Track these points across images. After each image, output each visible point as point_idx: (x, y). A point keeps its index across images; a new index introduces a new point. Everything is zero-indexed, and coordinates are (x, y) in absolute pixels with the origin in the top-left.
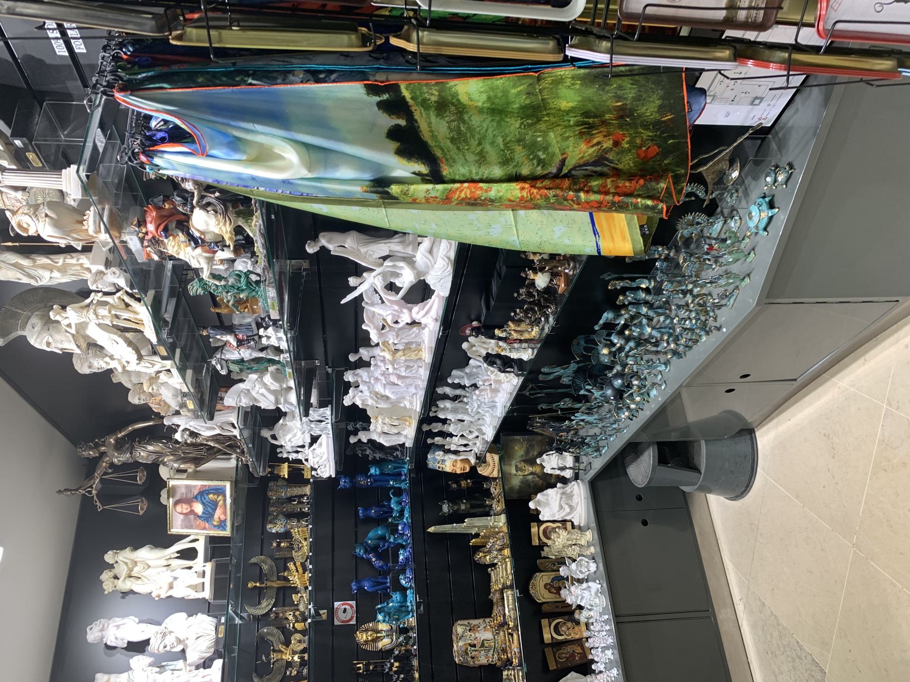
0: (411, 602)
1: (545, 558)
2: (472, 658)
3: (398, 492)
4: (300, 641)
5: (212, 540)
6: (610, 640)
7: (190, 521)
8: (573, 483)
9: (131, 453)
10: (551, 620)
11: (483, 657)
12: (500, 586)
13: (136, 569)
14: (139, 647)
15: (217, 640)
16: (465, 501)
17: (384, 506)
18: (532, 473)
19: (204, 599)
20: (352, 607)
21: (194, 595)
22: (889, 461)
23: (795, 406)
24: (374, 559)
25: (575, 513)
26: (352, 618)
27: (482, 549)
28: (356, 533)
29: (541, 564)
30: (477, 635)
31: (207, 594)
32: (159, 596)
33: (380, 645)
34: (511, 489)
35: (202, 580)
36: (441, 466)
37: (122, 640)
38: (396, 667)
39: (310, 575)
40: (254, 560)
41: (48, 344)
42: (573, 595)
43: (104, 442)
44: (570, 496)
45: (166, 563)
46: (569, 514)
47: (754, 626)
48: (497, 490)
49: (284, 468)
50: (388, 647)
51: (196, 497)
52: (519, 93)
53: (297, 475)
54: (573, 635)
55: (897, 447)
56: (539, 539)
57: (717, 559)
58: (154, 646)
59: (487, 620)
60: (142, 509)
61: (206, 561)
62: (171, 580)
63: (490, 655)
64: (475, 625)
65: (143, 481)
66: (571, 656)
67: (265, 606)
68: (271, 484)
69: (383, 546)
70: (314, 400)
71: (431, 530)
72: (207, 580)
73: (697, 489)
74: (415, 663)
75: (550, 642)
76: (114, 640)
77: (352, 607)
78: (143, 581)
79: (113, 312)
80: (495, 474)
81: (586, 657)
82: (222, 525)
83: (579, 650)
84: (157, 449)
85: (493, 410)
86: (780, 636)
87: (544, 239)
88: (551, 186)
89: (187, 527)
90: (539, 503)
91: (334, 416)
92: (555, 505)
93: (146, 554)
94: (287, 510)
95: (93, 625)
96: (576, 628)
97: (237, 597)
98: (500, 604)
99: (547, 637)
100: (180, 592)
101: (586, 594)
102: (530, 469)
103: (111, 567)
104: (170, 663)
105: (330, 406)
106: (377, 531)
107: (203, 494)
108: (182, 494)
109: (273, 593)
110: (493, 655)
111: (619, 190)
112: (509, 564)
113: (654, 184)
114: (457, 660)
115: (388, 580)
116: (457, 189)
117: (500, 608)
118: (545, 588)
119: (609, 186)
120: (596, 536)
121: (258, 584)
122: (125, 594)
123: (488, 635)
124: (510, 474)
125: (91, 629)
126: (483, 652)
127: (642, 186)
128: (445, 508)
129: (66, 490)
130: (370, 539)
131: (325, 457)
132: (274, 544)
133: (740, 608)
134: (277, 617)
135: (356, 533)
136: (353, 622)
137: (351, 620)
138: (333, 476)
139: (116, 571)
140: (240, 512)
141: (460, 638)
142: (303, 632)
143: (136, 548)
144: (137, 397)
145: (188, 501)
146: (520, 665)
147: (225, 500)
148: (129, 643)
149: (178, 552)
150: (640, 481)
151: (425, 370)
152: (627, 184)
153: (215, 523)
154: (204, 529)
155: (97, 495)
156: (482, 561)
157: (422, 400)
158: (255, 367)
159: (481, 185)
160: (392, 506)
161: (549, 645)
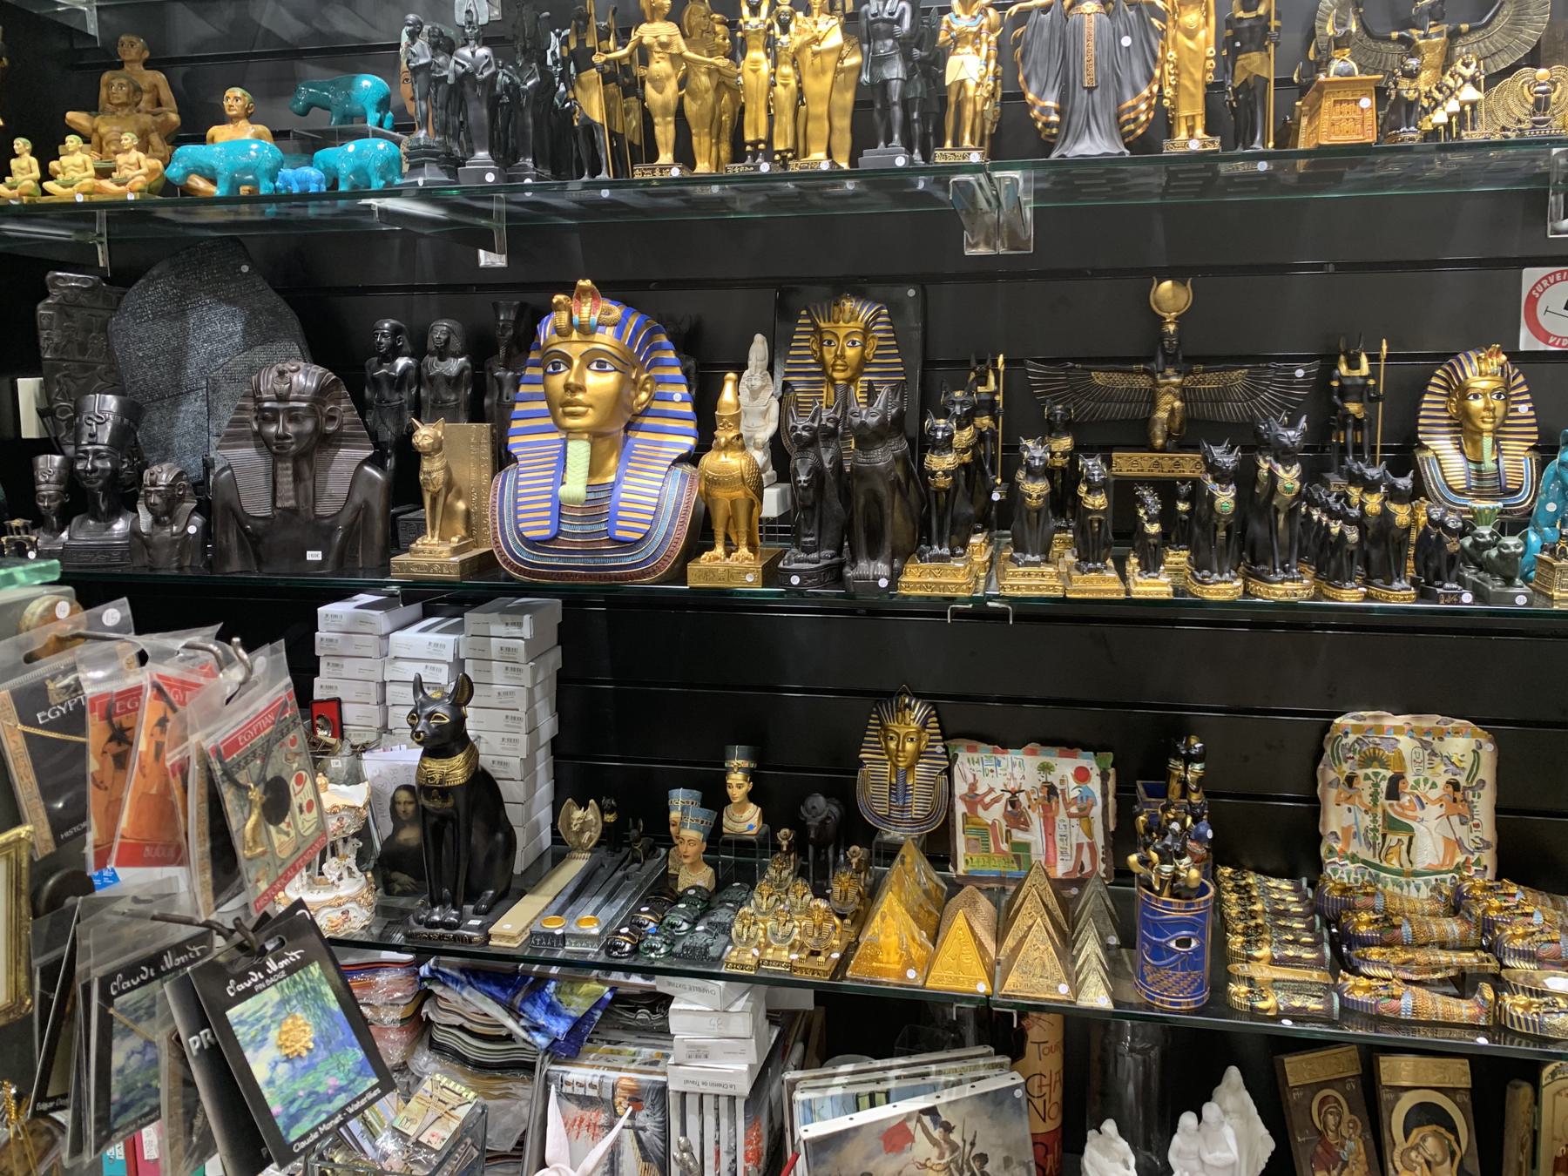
2: (1350, 780)
10: (1467, 1099)
11: (1348, 820)
30: (1434, 811)
38: (1273, 477)
52: (1266, 461)
59: (1488, 858)
63: (1355, 847)
64: (1471, 807)
66: (1328, 1148)
75: (1385, 1079)
123: (1429, 849)
136: (1527, 341)
137: (1539, 332)
141: (1425, 745)
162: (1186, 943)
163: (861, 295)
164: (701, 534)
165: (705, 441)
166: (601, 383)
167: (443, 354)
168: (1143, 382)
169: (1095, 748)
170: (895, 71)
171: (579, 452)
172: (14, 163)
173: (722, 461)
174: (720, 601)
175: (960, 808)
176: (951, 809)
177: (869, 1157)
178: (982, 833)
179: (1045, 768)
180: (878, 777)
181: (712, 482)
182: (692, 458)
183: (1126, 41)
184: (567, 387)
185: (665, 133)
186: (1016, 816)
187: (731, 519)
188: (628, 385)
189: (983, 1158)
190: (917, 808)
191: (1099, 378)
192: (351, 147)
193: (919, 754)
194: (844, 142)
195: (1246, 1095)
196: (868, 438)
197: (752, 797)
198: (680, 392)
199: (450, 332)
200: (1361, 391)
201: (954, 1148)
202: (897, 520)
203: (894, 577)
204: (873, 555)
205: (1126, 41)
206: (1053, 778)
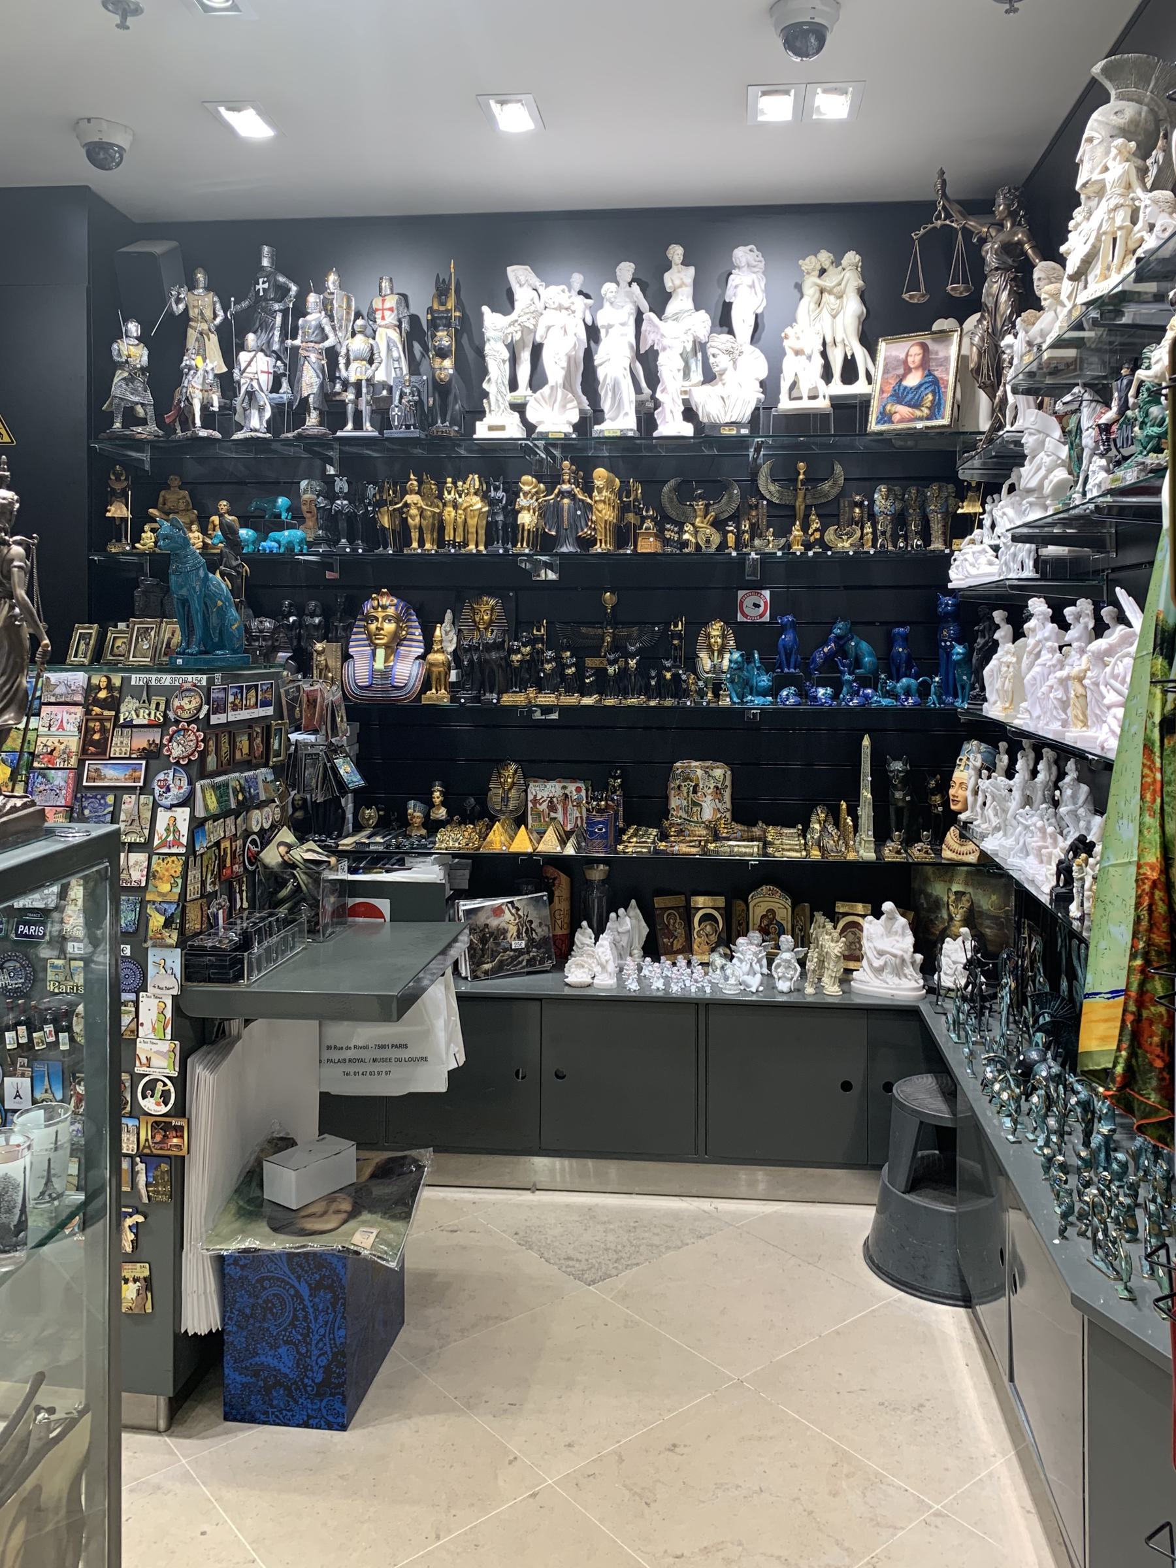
0: (752, 701)
1: (812, 917)
2: (679, 787)
3: (924, 691)
4: (708, 541)
5: (864, 403)
6: (675, 989)
7: (895, 369)
8: (921, 982)
9: (997, 269)
10: (723, 912)
11: (678, 802)
12: (770, 838)
13: (832, 298)
14: (724, 321)
15: (716, 426)
16: (908, 798)
17: (909, 667)
18: (951, 919)
19: (778, 401)
20: (761, 616)
21: (785, 386)
22: (847, 1476)
23: (988, 1382)
24: (826, 650)
25: (872, 975)
26: (746, 616)
27: (831, 819)
28: (872, 623)
29: (803, 909)
30: (709, 798)
31: (786, 404)
32: (786, 337)
33: (703, 655)
34: (926, 880)
35: (805, 396)
36: (963, 764)
37: (735, 295)
39: (798, 553)
40: (838, 469)
41: (1090, 140)
42: (748, 947)
43: (1020, 224)
44: (898, 971)
45: (838, 340)
46: (871, 965)
47: (676, 1215)
48: (917, 853)
49: (974, 506)
50: (699, 668)
51: (930, 374)
53: (963, 527)
54: (698, 940)
55: (864, 1493)
56: (845, 914)
57: (781, 1193)
58: (722, 340)
59: (728, 815)
60: (911, 297)
61: (832, 398)
62: (807, 351)
63: (681, 813)
64: (723, 796)
65: (952, 293)
66: (669, 930)
67: (769, 489)
68: (951, 488)
69: (843, 664)
70: (1052, 550)
71: (866, 742)
72: (805, 404)
73: (884, 1185)
74: (668, 702)
76: (734, 284)
77: (761, 616)
78: (814, 311)
79: (1119, 233)
80: (947, 854)
81: (665, 954)
82: (885, 417)
83: (677, 945)
84: (1002, 307)
85: (1021, 851)
86: (652, 1245)
87: (1109, 908)
88: (1156, 914)
89: (886, 365)
90: (892, 919)
91: (1016, 583)
92: (886, 944)
93: (853, 307)
94: (911, 515)
95: (757, 253)
96: (707, 947)
97: (782, 447)
98: (745, 835)
99: (700, 901)
100: (791, 367)
101: (746, 967)
102: (958, 917)
103: (837, 262)
104: (700, 364)
105: (1038, 576)
106: (870, 655)
107: (934, 383)
108: (937, 353)
109: (787, 501)
110: (680, 818)
111: (1145, 1024)
112: (798, 855)
113: (1154, 1083)
114: (678, 764)
115: (792, 670)
116: (1153, 762)
117: (739, 834)
118: (769, 911)
119: (1152, 1009)
120: (830, 1000)
121: (801, 477)
122: (799, 287)
123: (708, 814)
124: (951, 881)
125: (751, 251)
126: (685, 803)
127: (1151, 1064)
128: (897, 766)
129: (944, 182)
130: (857, 645)
131: (973, 571)
132: (858, 498)
133: (706, 1205)
134: (751, 507)
135: (872, 623)
136: (740, 618)
138: (950, 586)
139: (832, 271)
140: (910, 443)
141: (706, 772)
142: (723, 545)
143: (862, 295)
144: (1042, 275)
145: (925, 364)
146: (657, 851)
147: (921, 419)
148: (731, 304)
149: (853, 356)
150: (904, 1089)
151: (1055, 732)
152: (1156, 1039)
153: (888, 408)
154: (882, 391)
155: (935, 228)
156: (813, 818)
157: (1025, 728)
158: (1074, 454)
159: (1158, 800)
160: (904, 680)
161: (688, 901)
162: (600, 829)
163: (491, 595)
164: (426, 685)
165: (428, 649)
166: (389, 627)
167: (313, 615)
168: (600, 631)
169: (584, 780)
170: (500, 518)
171: (381, 653)
172: (143, 535)
173: (435, 657)
174: (434, 708)
175: (530, 805)
176: (526, 806)
177: (488, 918)
178: (538, 815)
179: (564, 788)
180: (496, 795)
181: (431, 665)
182: (423, 657)
183: (579, 513)
184: (377, 628)
185: (415, 535)
186: (552, 807)
187: (439, 679)
188: (399, 628)
189: (531, 922)
190: (512, 807)
191: (584, 630)
192: (286, 533)
193: (513, 784)
194: (482, 538)
195: (638, 911)
196: (488, 648)
197: (443, 804)
198: (418, 632)
199: (316, 606)
200: (678, 635)
201: (520, 917)
202: (500, 677)
203: (499, 700)
204: (491, 692)
205: (579, 513)
206: (567, 792)
